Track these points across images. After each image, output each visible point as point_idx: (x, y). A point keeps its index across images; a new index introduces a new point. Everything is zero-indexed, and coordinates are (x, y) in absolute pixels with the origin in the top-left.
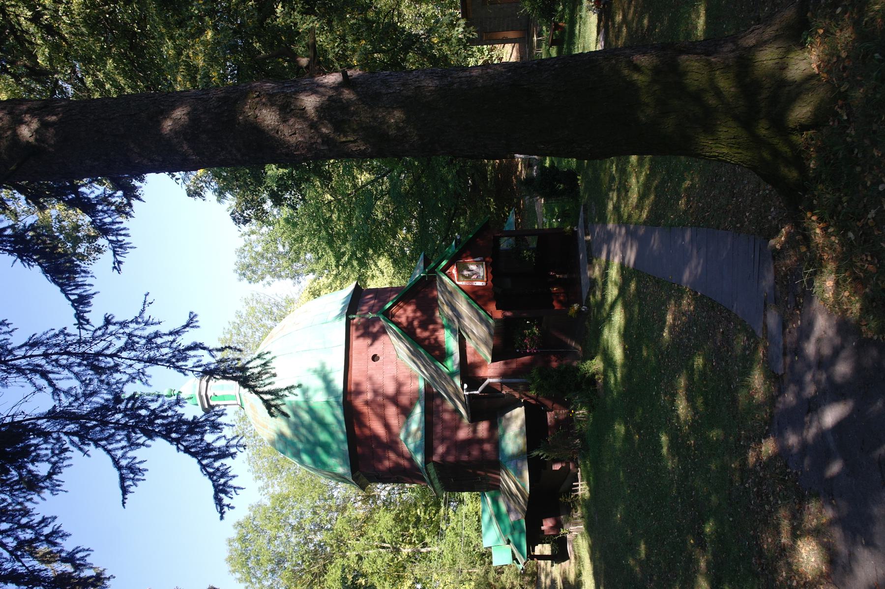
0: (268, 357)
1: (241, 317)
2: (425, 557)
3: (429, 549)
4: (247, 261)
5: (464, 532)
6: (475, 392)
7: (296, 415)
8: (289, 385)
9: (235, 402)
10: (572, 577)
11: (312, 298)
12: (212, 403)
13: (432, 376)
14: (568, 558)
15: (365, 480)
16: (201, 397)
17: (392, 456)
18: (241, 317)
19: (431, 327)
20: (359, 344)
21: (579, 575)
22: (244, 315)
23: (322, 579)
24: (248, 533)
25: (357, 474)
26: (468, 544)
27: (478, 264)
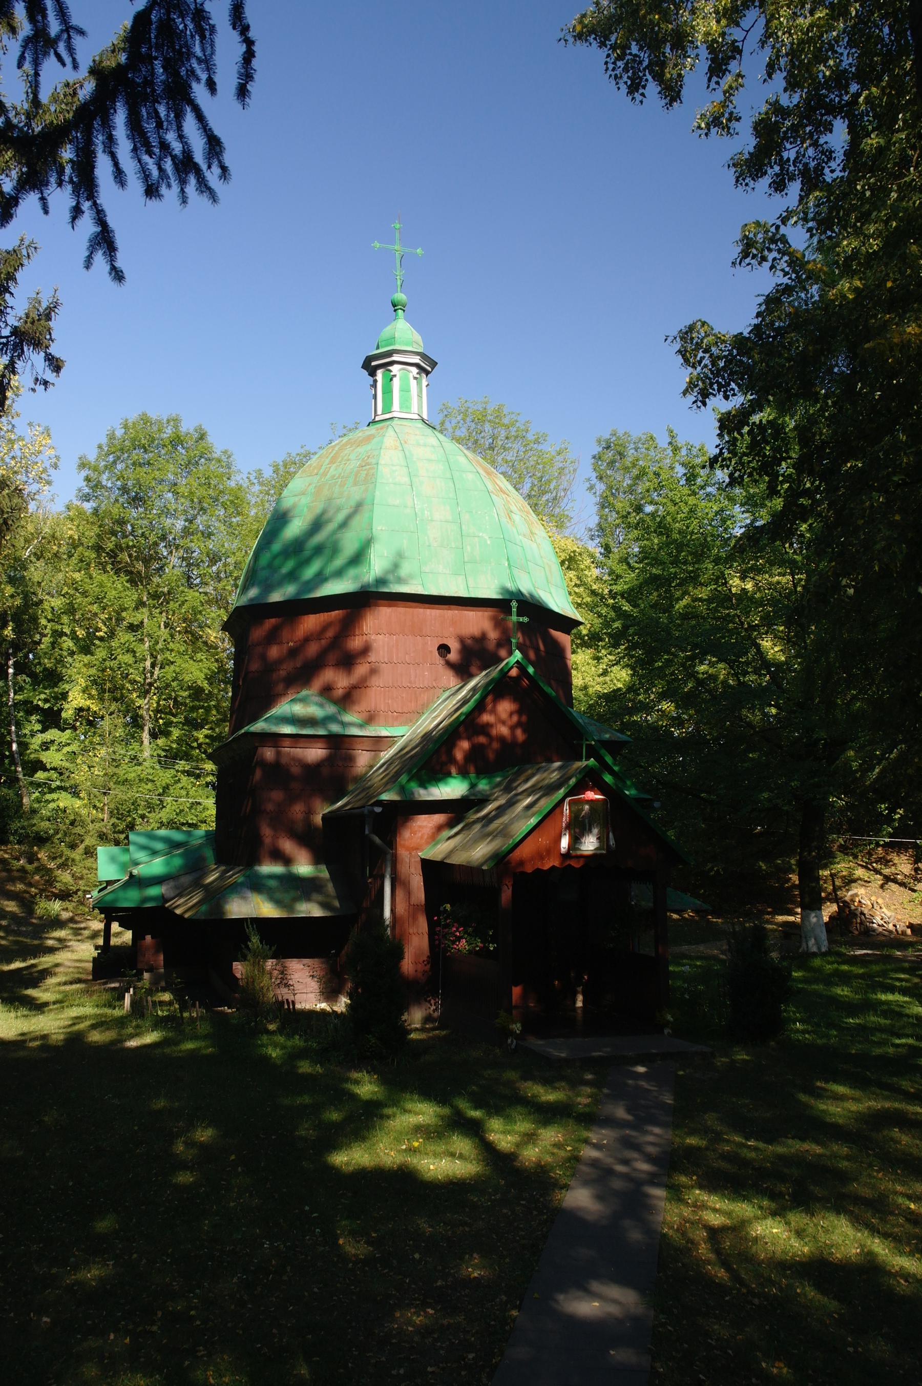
0: (212, 176)
1: (537, 442)
4: (631, 453)
5: (169, 799)
9: (379, 411)
11: (564, 556)
16: (390, 354)
18: (537, 442)
22: (540, 447)
23: (109, 567)
24: (187, 450)
26: (150, 807)
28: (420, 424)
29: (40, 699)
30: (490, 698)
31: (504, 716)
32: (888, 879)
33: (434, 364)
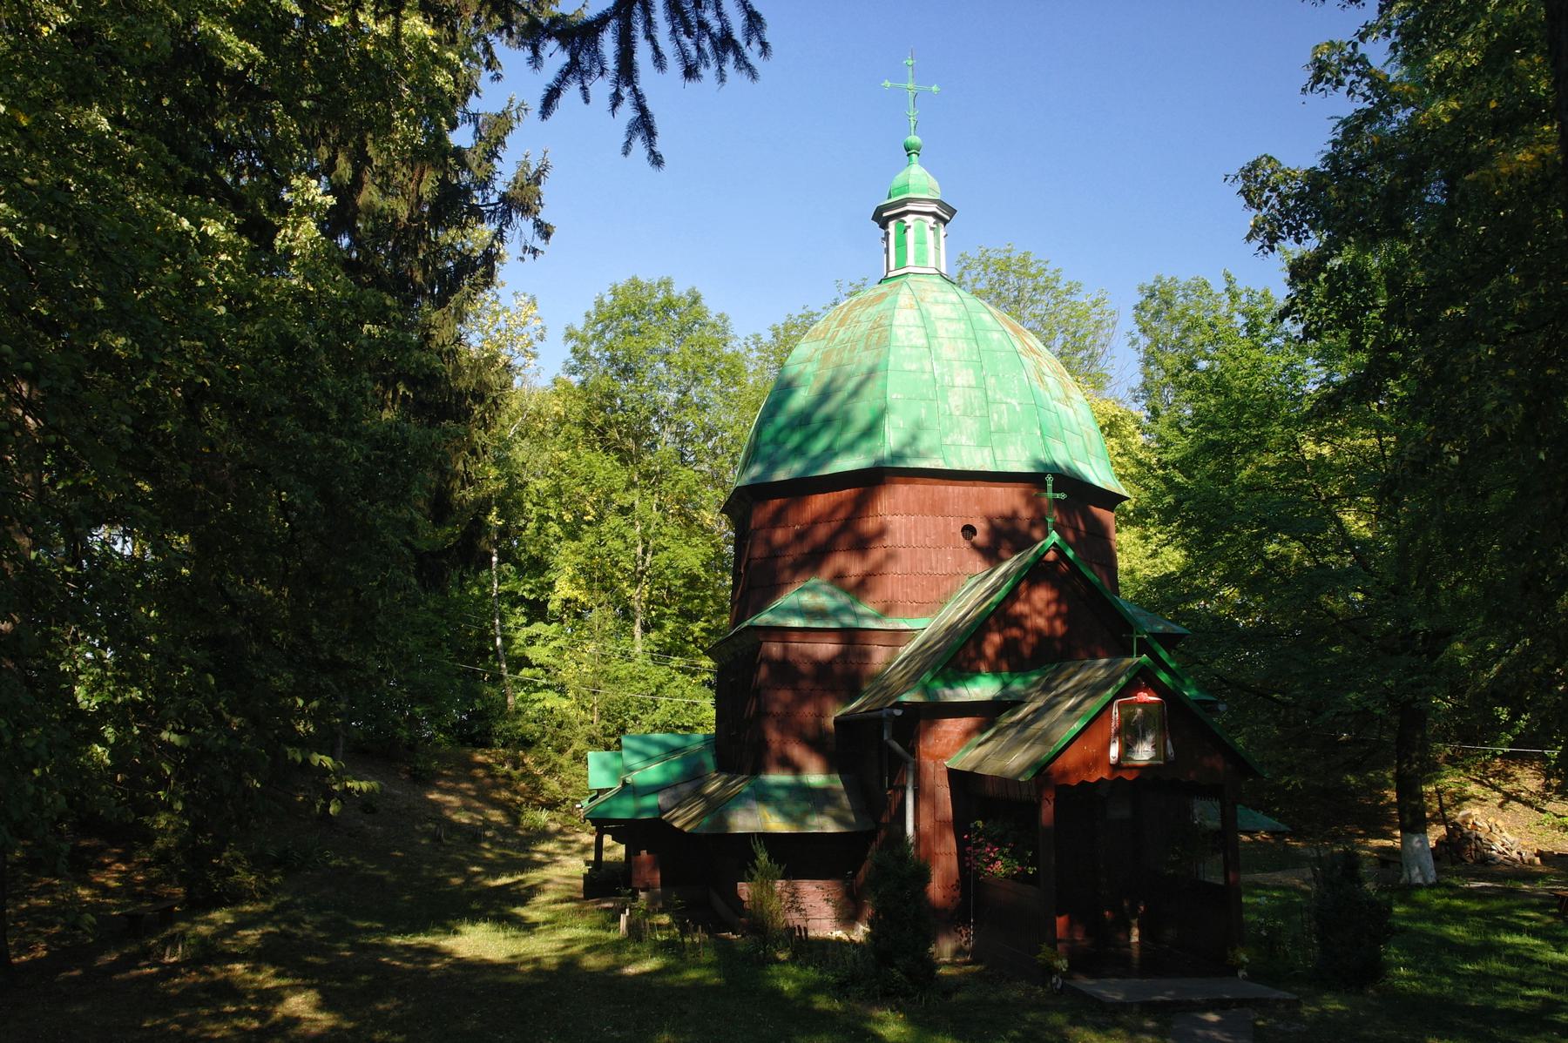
0: (752, 53)
1: (1069, 292)
2: (624, 630)
3: (638, 636)
8: (659, 124)
9: (892, 267)
11: (1103, 421)
12: (892, 225)
16: (903, 203)
18: (1069, 292)
23: (597, 445)
24: (680, 315)
26: (643, 708)
28: (938, 280)
29: (525, 590)
30: (1023, 585)
31: (1040, 605)
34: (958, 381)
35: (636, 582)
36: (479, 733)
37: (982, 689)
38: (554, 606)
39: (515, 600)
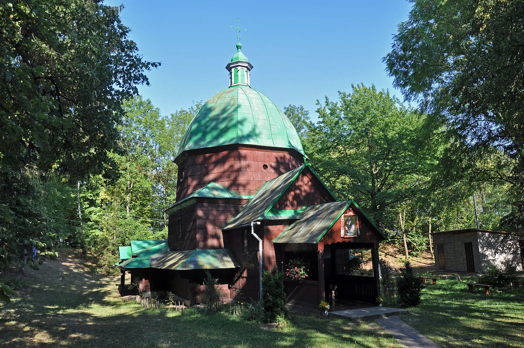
3: (128, 211)
4: (296, 113)
6: (253, 231)
7: (225, 119)
9: (233, 83)
10: (107, 299)
12: (233, 70)
13: (256, 205)
14: (122, 296)
15: (181, 161)
16: (237, 62)
17: (194, 183)
19: (295, 202)
20: (271, 158)
21: (108, 304)
24: (144, 107)
25: (187, 155)
27: (356, 232)
28: (248, 87)
29: (89, 195)
30: (301, 175)
31: (306, 182)
32: (386, 254)
33: (252, 67)
34: (261, 118)
35: (127, 193)
36: (73, 243)
37: (286, 214)
38: (98, 202)
39: (86, 199)
